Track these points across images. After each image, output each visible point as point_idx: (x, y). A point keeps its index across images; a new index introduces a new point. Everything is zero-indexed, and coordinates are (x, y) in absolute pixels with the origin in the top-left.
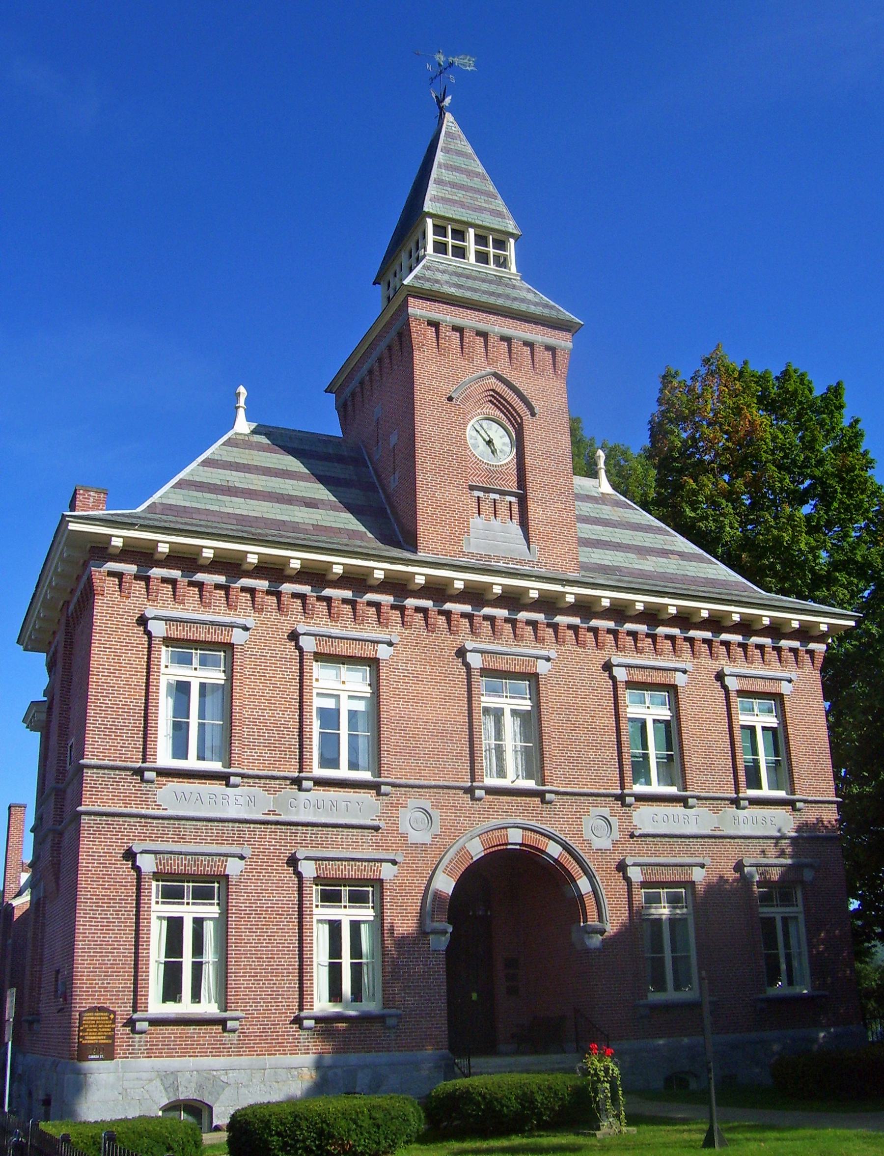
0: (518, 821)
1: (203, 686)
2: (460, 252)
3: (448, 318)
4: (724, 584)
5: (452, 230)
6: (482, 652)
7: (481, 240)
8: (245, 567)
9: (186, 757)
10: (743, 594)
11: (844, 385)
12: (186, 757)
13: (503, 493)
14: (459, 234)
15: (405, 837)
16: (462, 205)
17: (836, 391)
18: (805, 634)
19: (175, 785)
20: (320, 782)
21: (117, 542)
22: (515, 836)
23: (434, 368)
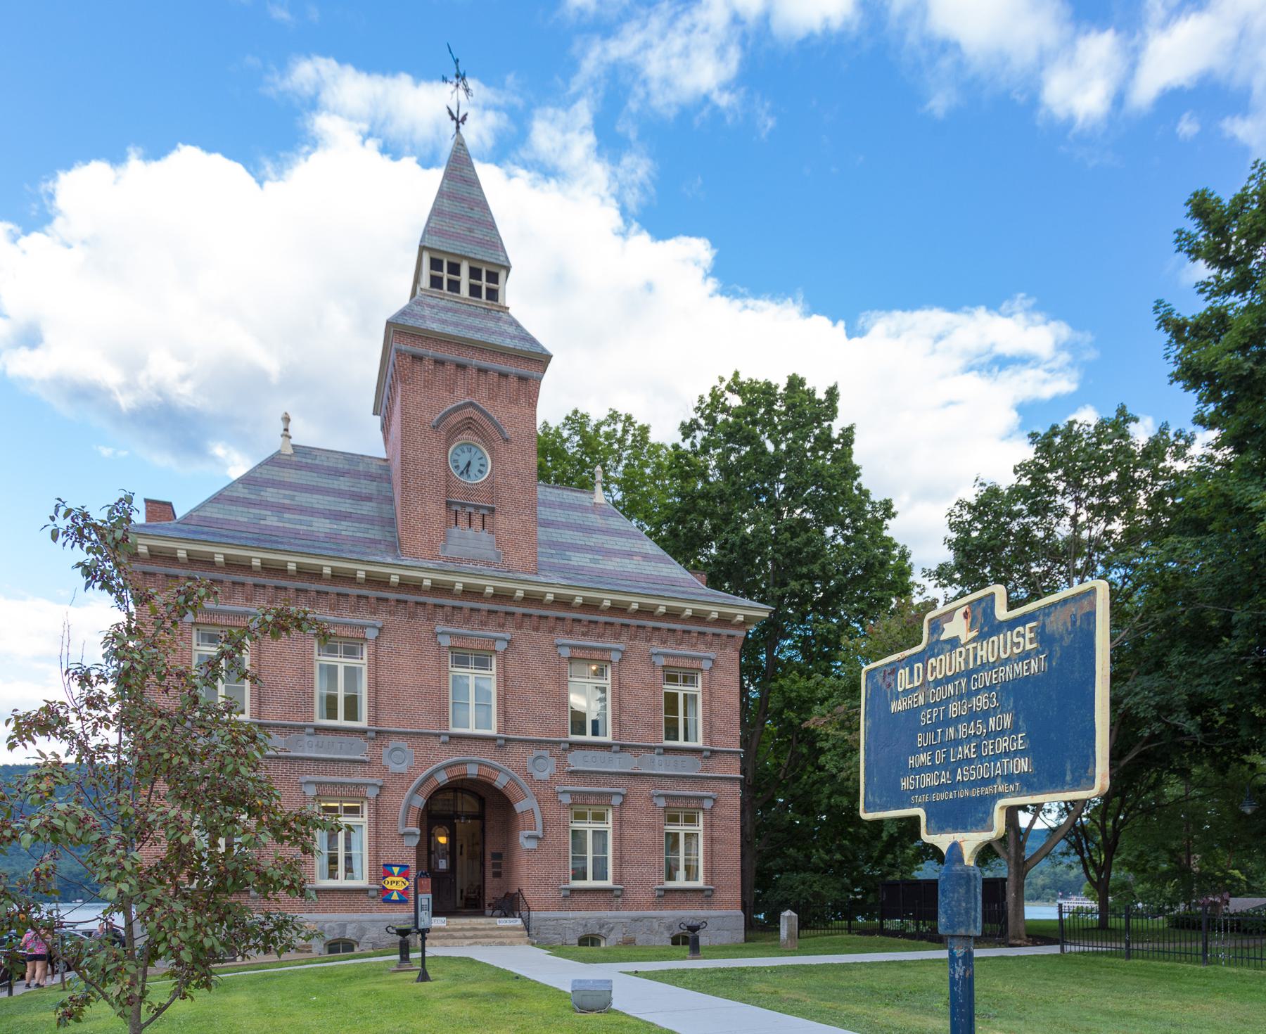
0: (475, 758)
1: (685, 695)
2: (454, 286)
3: (430, 352)
4: (671, 582)
5: (449, 263)
6: (451, 635)
7: (475, 273)
8: (574, 604)
9: (336, 718)
10: (689, 590)
11: (840, 389)
12: (336, 718)
13: (477, 507)
14: (454, 269)
15: (386, 768)
16: (457, 237)
17: (832, 394)
18: (724, 621)
19: (577, 753)
20: (319, 730)
21: (427, 583)
22: (472, 771)
23: (418, 399)
